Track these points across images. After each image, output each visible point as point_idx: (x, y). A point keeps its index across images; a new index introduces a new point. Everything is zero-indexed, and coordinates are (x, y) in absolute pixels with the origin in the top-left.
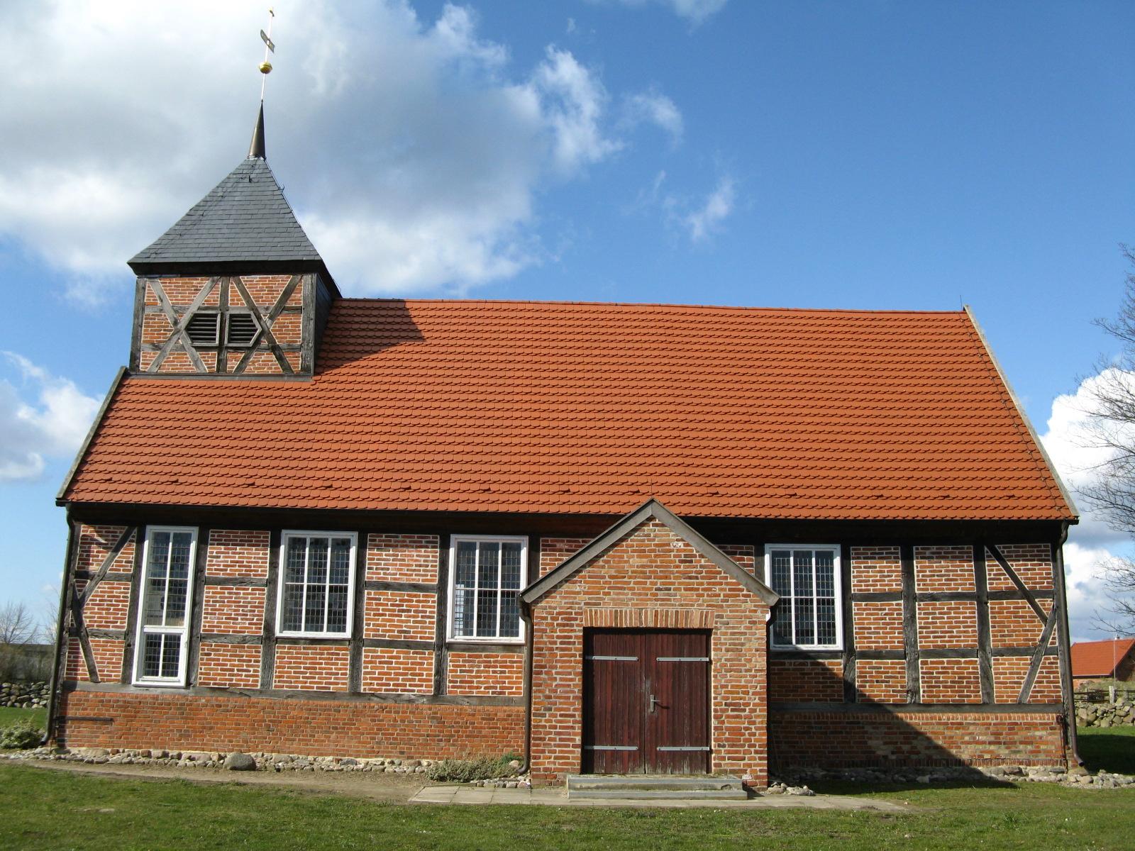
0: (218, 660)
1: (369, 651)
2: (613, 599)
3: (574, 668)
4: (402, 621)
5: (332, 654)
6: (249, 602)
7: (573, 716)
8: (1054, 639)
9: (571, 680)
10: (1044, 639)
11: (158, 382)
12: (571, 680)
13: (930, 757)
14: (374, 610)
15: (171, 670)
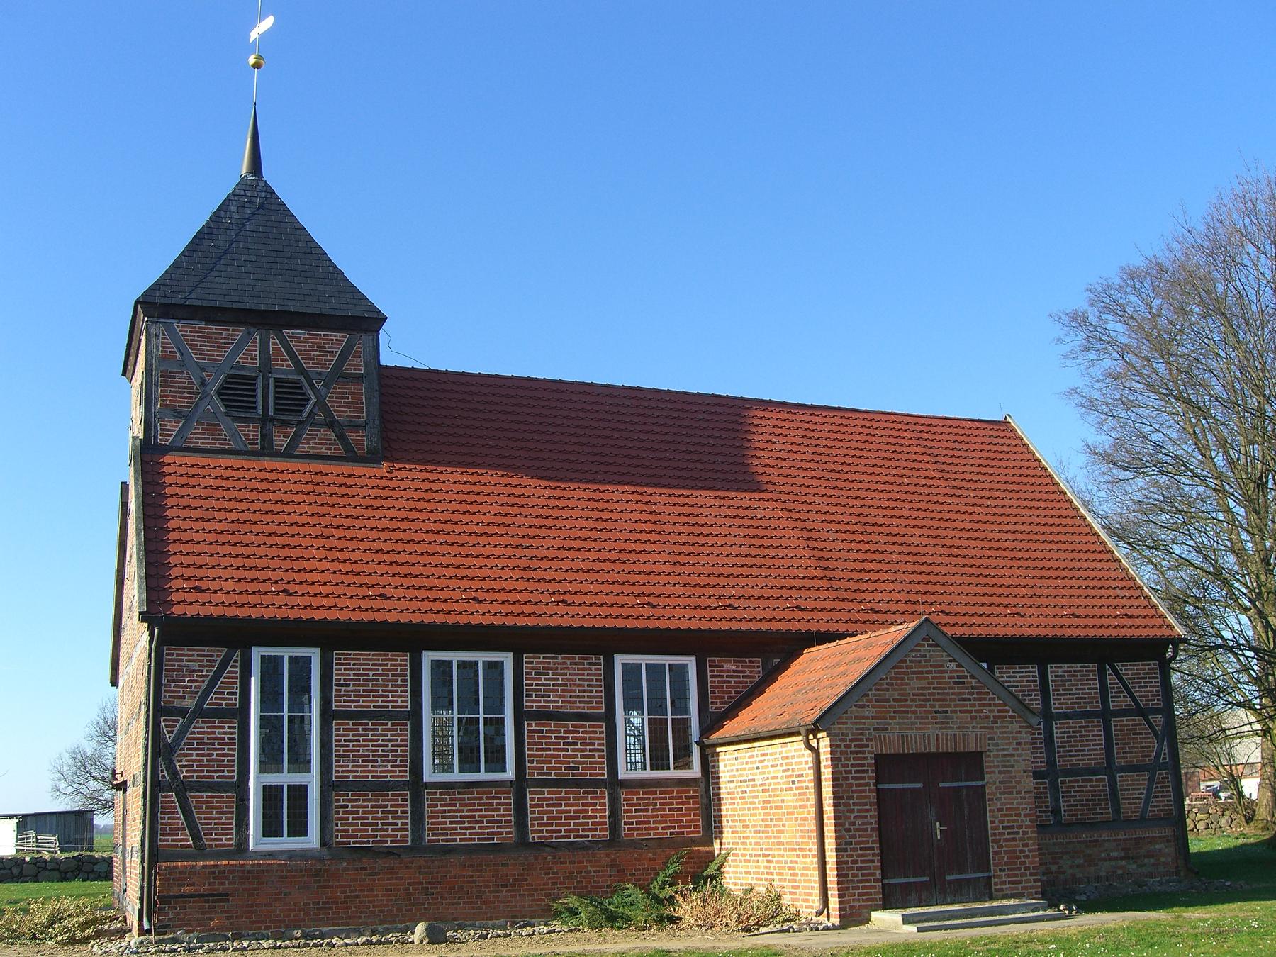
0: (358, 812)
1: (535, 793)
2: (899, 723)
3: (868, 797)
4: (569, 756)
5: (493, 798)
6: (389, 740)
7: (872, 849)
8: (1165, 757)
9: (868, 811)
10: (1158, 756)
11: (202, 461)
12: (868, 811)
13: (1073, 875)
14: (535, 744)
15: (299, 828)
